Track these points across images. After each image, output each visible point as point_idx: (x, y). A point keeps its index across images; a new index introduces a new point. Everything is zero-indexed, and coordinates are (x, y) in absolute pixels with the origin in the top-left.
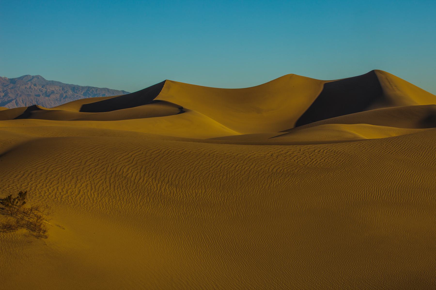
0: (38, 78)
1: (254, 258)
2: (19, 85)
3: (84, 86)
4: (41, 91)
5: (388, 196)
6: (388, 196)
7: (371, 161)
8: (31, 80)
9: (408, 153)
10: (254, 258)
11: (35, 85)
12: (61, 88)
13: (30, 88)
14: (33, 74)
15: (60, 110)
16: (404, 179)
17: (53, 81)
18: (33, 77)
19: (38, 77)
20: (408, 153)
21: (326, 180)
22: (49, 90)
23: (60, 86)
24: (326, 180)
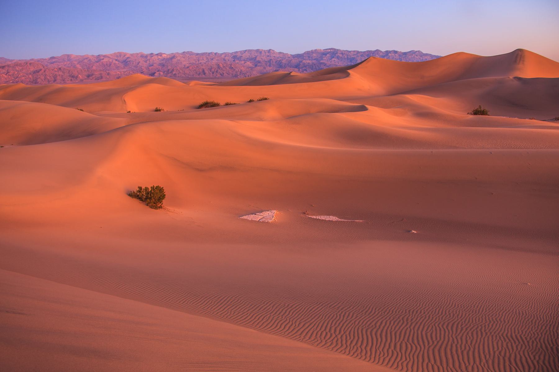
0: (419, 52)
1: (509, 340)
2: (408, 56)
3: (439, 55)
4: (420, 59)
5: (547, 316)
6: (547, 316)
7: (371, 309)
8: (415, 53)
9: (309, 308)
10: (509, 340)
11: (417, 56)
12: (431, 57)
13: (414, 57)
14: (416, 50)
15: (328, 75)
16: (548, 308)
17: (427, 54)
18: (416, 51)
19: (419, 51)
20: (309, 308)
21: (437, 305)
22: (424, 59)
23: (430, 56)
24: (437, 305)
